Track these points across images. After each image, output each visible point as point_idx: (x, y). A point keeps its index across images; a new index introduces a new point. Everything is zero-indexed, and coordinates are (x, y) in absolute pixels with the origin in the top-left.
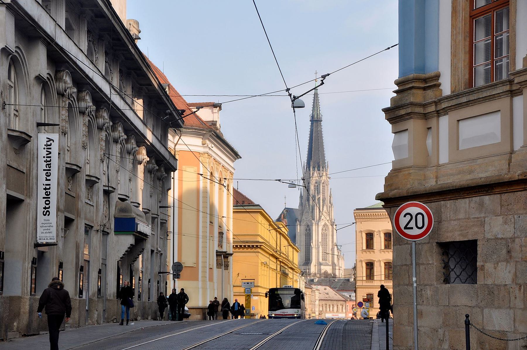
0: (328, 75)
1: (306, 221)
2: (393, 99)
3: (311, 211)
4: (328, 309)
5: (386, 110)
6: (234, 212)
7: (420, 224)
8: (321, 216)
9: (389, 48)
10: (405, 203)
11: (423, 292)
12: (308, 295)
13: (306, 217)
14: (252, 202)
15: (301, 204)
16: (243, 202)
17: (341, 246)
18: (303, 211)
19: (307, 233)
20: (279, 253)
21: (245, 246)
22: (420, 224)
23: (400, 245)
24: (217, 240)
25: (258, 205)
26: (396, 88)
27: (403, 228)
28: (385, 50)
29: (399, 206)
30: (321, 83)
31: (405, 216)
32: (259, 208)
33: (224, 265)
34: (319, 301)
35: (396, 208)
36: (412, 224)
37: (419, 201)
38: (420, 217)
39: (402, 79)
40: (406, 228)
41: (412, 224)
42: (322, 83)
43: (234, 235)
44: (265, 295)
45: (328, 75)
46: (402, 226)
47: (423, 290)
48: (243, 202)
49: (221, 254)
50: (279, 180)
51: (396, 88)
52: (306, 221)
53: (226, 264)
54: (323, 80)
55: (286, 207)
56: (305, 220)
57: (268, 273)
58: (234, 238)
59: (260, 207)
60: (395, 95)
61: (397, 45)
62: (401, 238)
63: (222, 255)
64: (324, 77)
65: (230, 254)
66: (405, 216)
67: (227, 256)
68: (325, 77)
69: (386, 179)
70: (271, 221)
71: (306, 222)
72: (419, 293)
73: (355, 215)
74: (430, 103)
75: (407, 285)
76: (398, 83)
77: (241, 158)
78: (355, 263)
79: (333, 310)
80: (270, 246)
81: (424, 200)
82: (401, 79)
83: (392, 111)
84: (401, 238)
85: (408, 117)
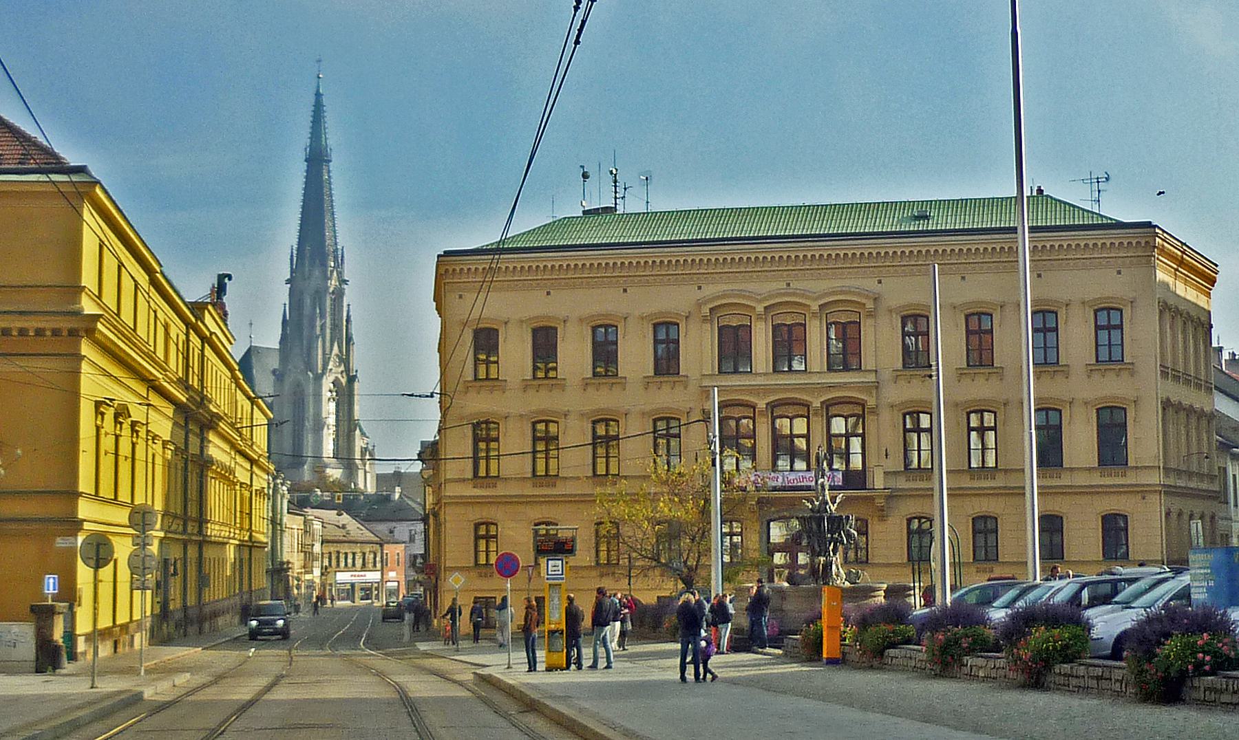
4: (342, 564)
12: (296, 530)
34: (322, 544)
79: (354, 565)
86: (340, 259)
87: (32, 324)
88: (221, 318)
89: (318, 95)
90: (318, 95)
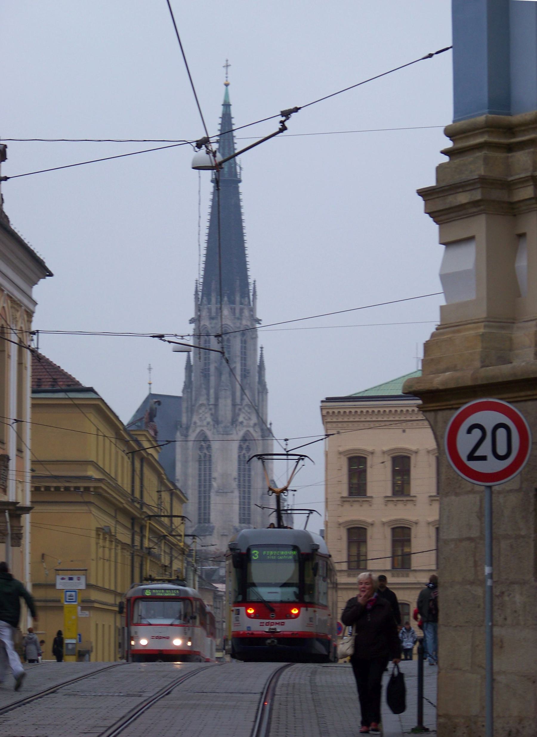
0: (296, 110)
1: (201, 426)
2: (440, 169)
3: (212, 401)
5: (424, 193)
6: (34, 406)
7: (502, 450)
8: (239, 415)
9: (430, 56)
10: (473, 400)
11: (506, 598)
13: (201, 416)
14: (78, 383)
15: (188, 386)
16: (55, 381)
17: (295, 491)
18: (193, 402)
19: (202, 457)
20: (138, 506)
21: (57, 489)
22: (502, 450)
23: (457, 494)
24: (10, 472)
25: (91, 390)
26: (449, 144)
27: (464, 457)
28: (422, 59)
29: (457, 409)
30: (281, 127)
31: (469, 431)
32: (94, 396)
33: (12, 534)
35: (453, 411)
36: (485, 449)
37: (500, 396)
38: (501, 433)
39: (463, 123)
40: (471, 457)
41: (485, 449)
42: (283, 128)
43: (33, 462)
44: (117, 609)
45: (296, 110)
46: (464, 453)
47: (506, 594)
48: (55, 381)
49: (6, 507)
50: (161, 337)
51: (449, 144)
52: (201, 426)
53: (15, 532)
54: (285, 121)
55: (152, 393)
56: (199, 423)
57: (113, 554)
58: (33, 470)
59: (96, 393)
60: (446, 159)
61: (447, 49)
62: (460, 478)
63: (7, 511)
64: (286, 114)
65: (26, 507)
66: (469, 431)
67: (18, 512)
68: (290, 115)
69: (427, 346)
70: (121, 427)
71: (202, 428)
72: (497, 601)
73: (325, 412)
74: (523, 179)
75: (472, 583)
76: (450, 133)
77: (51, 275)
78: (323, 528)
80: (118, 489)
81: (510, 395)
82: (459, 124)
83: (440, 195)
84: (460, 478)
85: (475, 210)
86: (251, 294)
87: (62, 484)
88: (153, 437)
89: (227, 105)
90: (227, 105)
